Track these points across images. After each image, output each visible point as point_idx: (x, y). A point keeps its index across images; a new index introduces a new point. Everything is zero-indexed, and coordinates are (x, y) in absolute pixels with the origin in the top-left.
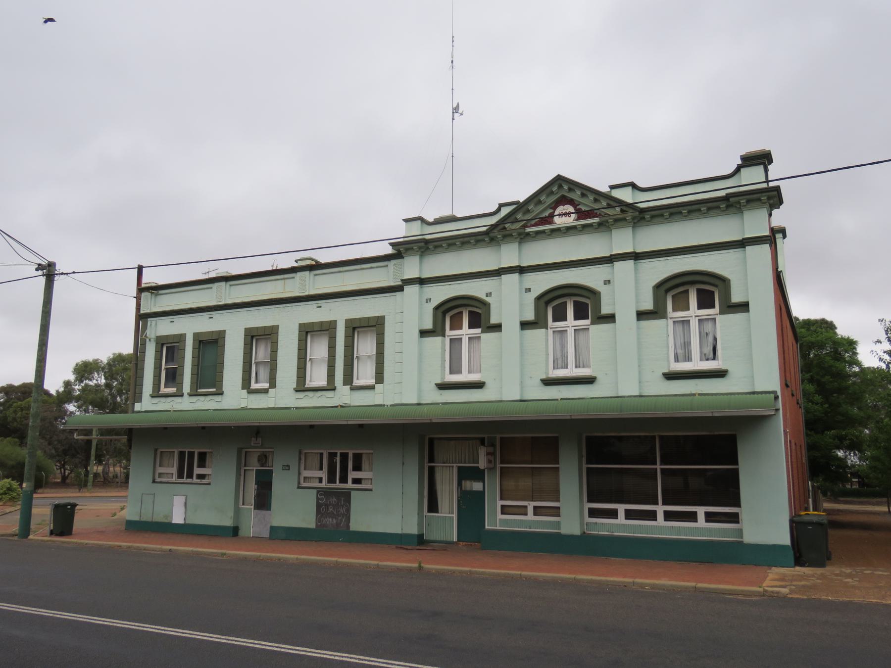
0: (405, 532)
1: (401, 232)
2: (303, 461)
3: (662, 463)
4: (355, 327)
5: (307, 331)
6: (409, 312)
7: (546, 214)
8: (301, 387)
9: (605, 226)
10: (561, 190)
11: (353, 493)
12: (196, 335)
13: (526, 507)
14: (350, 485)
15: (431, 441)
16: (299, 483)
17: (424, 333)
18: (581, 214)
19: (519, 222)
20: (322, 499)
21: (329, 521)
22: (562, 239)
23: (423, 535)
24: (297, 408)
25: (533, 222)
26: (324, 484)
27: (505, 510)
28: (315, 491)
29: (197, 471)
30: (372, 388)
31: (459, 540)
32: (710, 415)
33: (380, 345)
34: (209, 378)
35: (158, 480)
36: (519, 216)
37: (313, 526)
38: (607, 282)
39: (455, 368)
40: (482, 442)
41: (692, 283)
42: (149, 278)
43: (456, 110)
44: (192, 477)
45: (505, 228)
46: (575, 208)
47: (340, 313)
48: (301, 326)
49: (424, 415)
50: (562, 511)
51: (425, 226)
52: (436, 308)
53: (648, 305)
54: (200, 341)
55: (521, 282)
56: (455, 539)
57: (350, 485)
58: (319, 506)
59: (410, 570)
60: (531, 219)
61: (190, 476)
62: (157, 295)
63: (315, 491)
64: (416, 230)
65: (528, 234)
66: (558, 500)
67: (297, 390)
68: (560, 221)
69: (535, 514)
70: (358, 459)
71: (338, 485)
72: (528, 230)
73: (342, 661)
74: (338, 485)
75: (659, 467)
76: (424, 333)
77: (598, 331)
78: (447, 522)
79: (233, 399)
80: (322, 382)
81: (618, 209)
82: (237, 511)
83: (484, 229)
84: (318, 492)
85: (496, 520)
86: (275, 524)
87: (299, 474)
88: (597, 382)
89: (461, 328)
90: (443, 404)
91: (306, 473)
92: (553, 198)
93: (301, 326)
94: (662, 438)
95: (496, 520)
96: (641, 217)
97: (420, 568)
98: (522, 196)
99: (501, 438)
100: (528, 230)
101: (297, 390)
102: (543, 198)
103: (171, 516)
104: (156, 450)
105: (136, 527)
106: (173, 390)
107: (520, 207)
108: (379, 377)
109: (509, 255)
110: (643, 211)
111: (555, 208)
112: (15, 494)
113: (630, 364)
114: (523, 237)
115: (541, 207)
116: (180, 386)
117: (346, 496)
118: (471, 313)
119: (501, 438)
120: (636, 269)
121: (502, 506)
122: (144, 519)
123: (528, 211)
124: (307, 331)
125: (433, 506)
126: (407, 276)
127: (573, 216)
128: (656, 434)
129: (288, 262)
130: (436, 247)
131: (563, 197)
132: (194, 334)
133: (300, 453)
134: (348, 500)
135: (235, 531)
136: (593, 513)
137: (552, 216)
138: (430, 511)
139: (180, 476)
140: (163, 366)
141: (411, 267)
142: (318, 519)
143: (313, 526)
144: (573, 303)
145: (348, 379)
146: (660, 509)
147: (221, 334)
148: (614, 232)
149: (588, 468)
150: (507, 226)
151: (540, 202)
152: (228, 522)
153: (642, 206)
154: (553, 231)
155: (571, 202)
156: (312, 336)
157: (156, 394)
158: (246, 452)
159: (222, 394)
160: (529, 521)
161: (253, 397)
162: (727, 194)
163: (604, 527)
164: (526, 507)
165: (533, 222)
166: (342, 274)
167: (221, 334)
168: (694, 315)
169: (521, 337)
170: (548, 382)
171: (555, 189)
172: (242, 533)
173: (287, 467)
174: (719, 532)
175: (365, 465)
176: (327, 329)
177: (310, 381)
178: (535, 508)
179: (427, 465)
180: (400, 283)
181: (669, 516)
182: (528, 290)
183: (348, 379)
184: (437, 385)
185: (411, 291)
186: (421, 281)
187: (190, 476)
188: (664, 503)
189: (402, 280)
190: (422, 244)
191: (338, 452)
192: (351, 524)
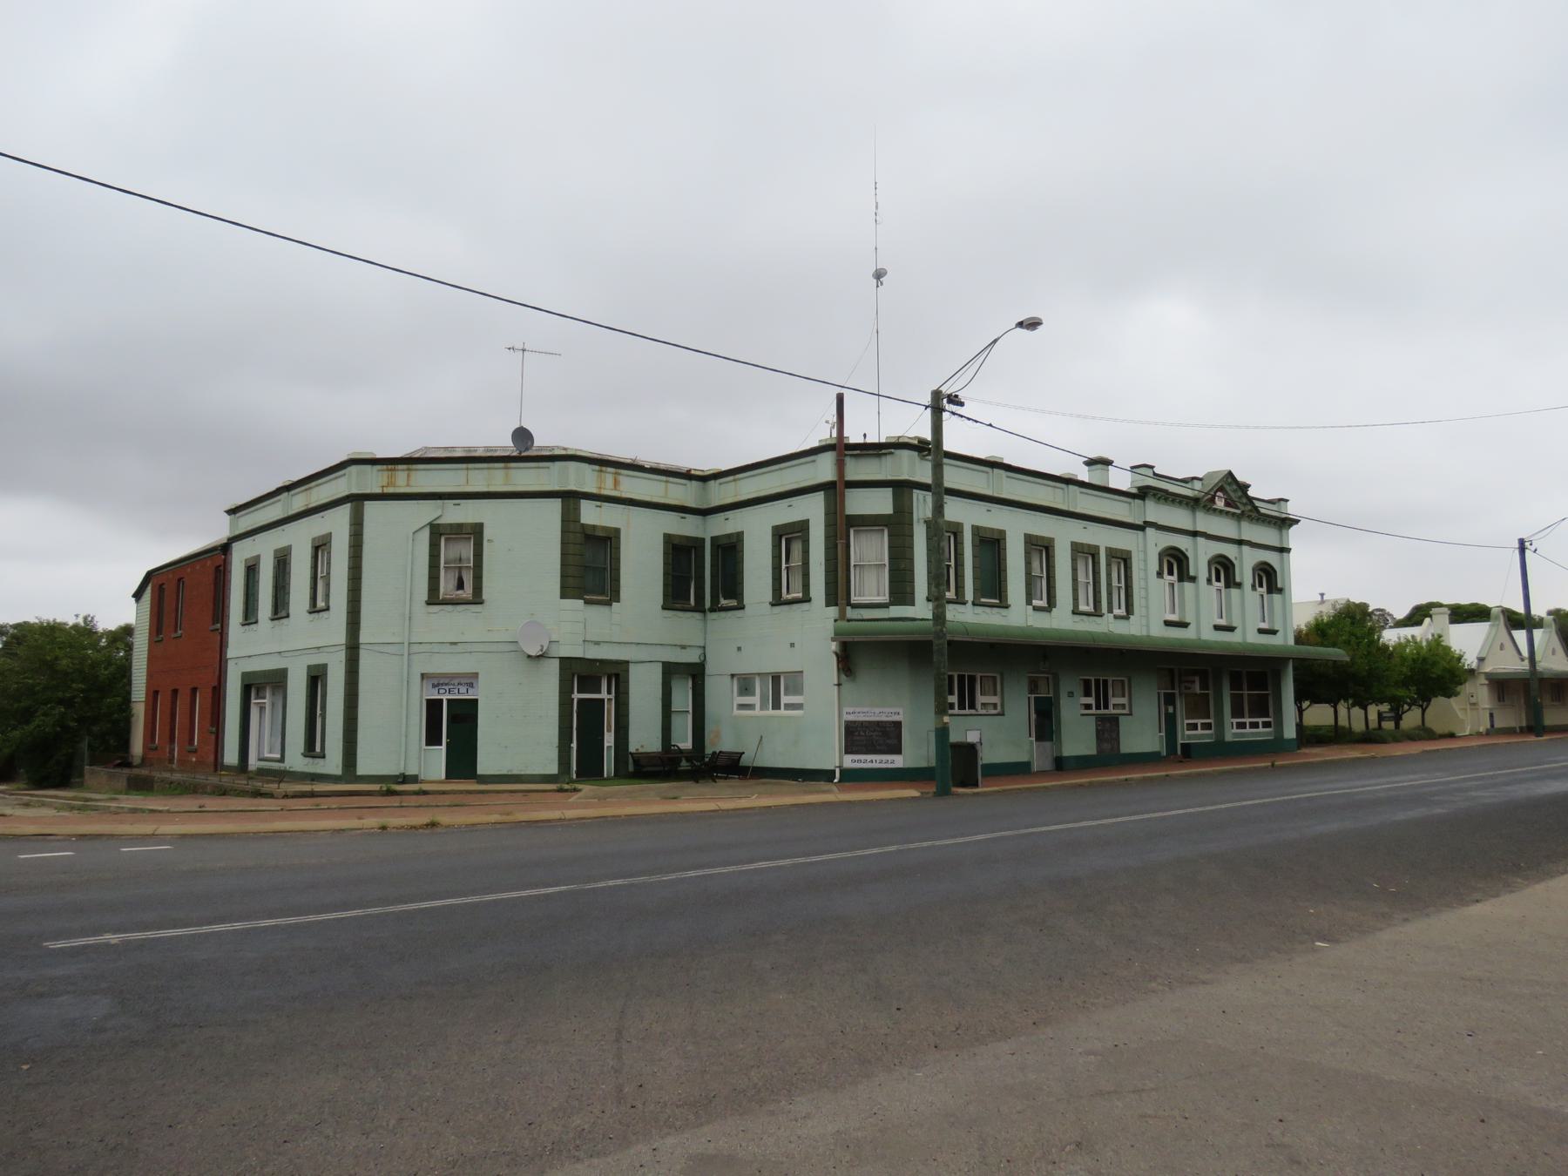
8: (1076, 612)
9: (1239, 518)
21: (1106, 746)
26: (1093, 711)
37: (1094, 752)
40: (1195, 673)
61: (972, 706)
67: (429, 603)
71: (1102, 711)
74: (771, 712)
79: (1018, 615)
80: (1090, 608)
117: (1115, 720)
126: (1150, 519)
139: (962, 707)
143: (1094, 752)
160: (1201, 735)
163: (1192, 732)
173: (1071, 694)
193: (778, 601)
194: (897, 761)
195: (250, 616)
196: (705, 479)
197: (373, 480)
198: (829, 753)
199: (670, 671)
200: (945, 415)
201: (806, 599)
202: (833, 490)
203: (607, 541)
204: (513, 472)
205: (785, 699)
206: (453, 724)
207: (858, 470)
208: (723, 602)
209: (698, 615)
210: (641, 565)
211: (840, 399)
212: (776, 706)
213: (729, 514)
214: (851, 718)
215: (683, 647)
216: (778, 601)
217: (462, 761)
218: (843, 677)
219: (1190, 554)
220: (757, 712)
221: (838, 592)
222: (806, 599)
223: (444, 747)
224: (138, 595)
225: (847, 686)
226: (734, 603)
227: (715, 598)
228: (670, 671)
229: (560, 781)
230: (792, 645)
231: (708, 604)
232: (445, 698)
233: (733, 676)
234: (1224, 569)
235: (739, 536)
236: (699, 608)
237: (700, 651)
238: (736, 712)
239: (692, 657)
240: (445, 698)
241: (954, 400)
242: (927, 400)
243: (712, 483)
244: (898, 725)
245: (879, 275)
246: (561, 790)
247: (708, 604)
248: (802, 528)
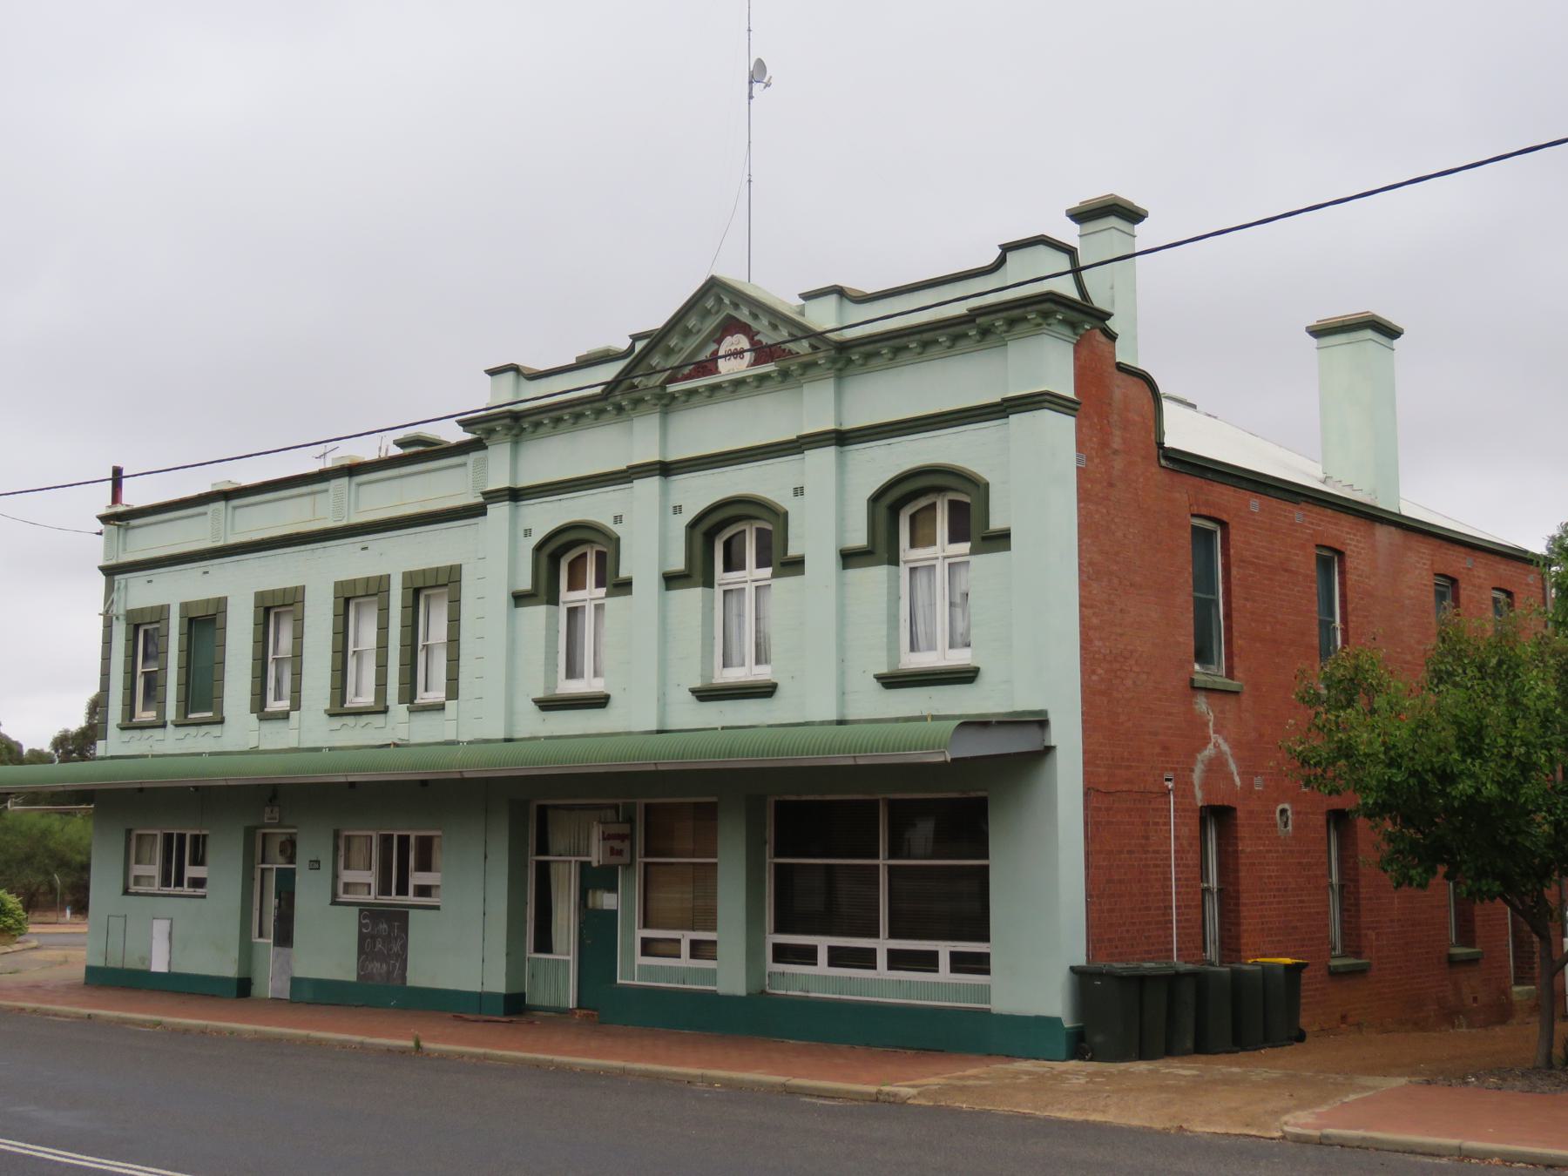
0: (486, 989)
1: (484, 396)
2: (342, 852)
3: (893, 854)
4: (419, 588)
5: (347, 598)
6: (494, 555)
7: (705, 354)
8: (339, 709)
10: (717, 308)
11: (412, 913)
12: (185, 607)
13: (678, 941)
14: (410, 898)
15: (543, 811)
16: (335, 894)
17: (519, 599)
18: (763, 353)
19: (652, 373)
20: (366, 926)
21: (377, 967)
22: (730, 404)
23: (523, 995)
24: (331, 749)
25: (686, 371)
26: (371, 898)
27: (648, 947)
28: (356, 910)
29: (191, 872)
30: (440, 707)
31: (579, 1007)
32: (851, 762)
33: (454, 621)
34: (201, 696)
35: (133, 889)
36: (655, 360)
37: (353, 977)
38: (799, 491)
39: (572, 672)
41: (940, 490)
42: (136, 495)
43: (758, 73)
44: (179, 883)
45: (634, 387)
46: (751, 339)
47: (396, 558)
48: (339, 586)
49: (664, 755)
50: (720, 950)
51: (523, 381)
52: (692, 526)
53: (858, 537)
54: (191, 620)
55: (664, 493)
56: (572, 1003)
57: (410, 898)
59: (403, 1052)
60: (680, 367)
62: (127, 529)
63: (356, 910)
64: (502, 394)
65: (673, 397)
66: (714, 929)
68: (730, 368)
69: (693, 956)
70: (426, 845)
71: (394, 899)
72: (672, 388)
73: (57, 1163)
75: (883, 862)
76: (519, 599)
77: (784, 586)
78: (559, 976)
80: (368, 699)
81: (805, 343)
82: (247, 951)
83: (598, 390)
84: (361, 911)
85: (635, 969)
86: (299, 973)
87: (336, 877)
88: (779, 693)
89: (584, 587)
90: (546, 738)
91: (347, 876)
92: (711, 323)
93: (339, 586)
94: (893, 805)
95: (635, 969)
96: (847, 357)
98: (657, 321)
99: (647, 806)
100: (672, 388)
101: (123, 729)
102: (692, 322)
103: (147, 958)
104: (129, 832)
105: (103, 979)
106: (150, 716)
107: (656, 340)
108: (453, 692)
109: (639, 440)
110: (843, 347)
111: (719, 342)
112: (11, 921)
113: (825, 662)
114: (667, 404)
115: (693, 342)
116: (162, 712)
117: (400, 918)
118: (952, 504)
119: (647, 806)
120: (841, 466)
121: (776, 947)
122: (111, 965)
123: (669, 352)
124: (347, 598)
125: (544, 943)
127: (748, 356)
128: (880, 797)
129: (307, 463)
130: (868, 357)
131: (730, 318)
132: (257, 594)
133: (337, 835)
134: (404, 929)
135: (243, 987)
136: (783, 954)
137: (715, 357)
138: (537, 950)
139: (166, 882)
140: (140, 669)
141: (499, 466)
142: (361, 966)
143: (353, 977)
144: (737, 536)
145: (409, 693)
146: (882, 945)
147: (221, 604)
148: (805, 386)
149: (777, 866)
150: (636, 381)
151: (687, 333)
152: (230, 970)
154: (714, 389)
155: (745, 329)
156: (358, 606)
157: (129, 724)
158: (264, 835)
159: (222, 722)
160: (678, 971)
161: (269, 727)
162: (971, 310)
163: (820, 979)
164: (678, 941)
165: (686, 371)
166: (395, 483)
167: (221, 604)
168: (940, 554)
169: (841, 585)
170: (893, 681)
171: (710, 303)
172: (256, 991)
173: (315, 865)
174: (940, 986)
175: (438, 858)
176: (376, 589)
177: (357, 695)
178: (831, 949)
179: (533, 859)
180: (481, 499)
181: (898, 960)
182: (678, 510)
183: (409, 693)
184: (536, 701)
185: (499, 512)
186: (515, 495)
188: (893, 935)
189: (484, 494)
190: (507, 421)
192: (408, 974)
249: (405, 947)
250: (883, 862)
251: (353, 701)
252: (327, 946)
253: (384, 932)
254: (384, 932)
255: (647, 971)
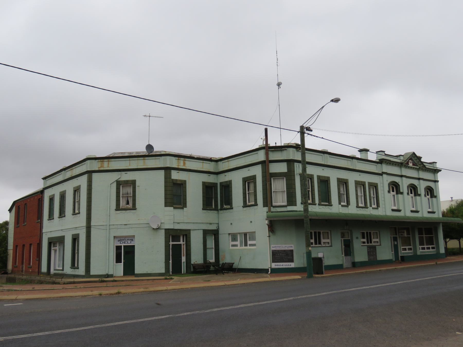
6: (383, 183)
8: (358, 207)
26: (366, 244)
34: (326, 198)
37: (367, 260)
40: (404, 229)
47: (367, 179)
58: (368, 252)
61: (320, 243)
74: (244, 247)
79: (336, 209)
80: (363, 205)
97: (436, 264)
139: (316, 244)
143: (367, 260)
153: (427, 167)
159: (232, 209)
163: (404, 252)
173: (357, 238)
187: (320, 243)
188: (181, 244)
191: (322, 232)
193: (245, 206)
194: (292, 265)
195: (51, 217)
196: (217, 161)
197: (95, 166)
198: (266, 262)
199: (206, 233)
200: (305, 135)
201: (256, 205)
202: (265, 164)
203: (182, 185)
204: (146, 161)
205: (249, 242)
206: (126, 255)
207: (274, 156)
208: (225, 206)
209: (216, 212)
210: (194, 194)
211: (266, 130)
212: (246, 245)
213: (226, 174)
214: (274, 249)
215: (211, 224)
216: (245, 206)
217: (129, 269)
218: (271, 233)
219: (400, 184)
220: (239, 247)
221: (268, 202)
222: (256, 205)
223: (122, 264)
224: (10, 210)
225: (272, 237)
226: (229, 207)
227: (222, 206)
228: (206, 233)
229: (166, 275)
230: (251, 222)
231: (219, 207)
232: (122, 245)
233: (229, 234)
234: (413, 189)
235: (230, 182)
236: (216, 209)
237: (217, 225)
238: (231, 248)
239: (214, 227)
240: (122, 245)
241: (309, 129)
242: (298, 129)
243: (220, 162)
244: (292, 251)
245: (279, 84)
246: (166, 279)
247: (219, 207)
248: (253, 178)
249: (376, 253)
250: (424, 236)
251: (360, 205)
252: (361, 254)
253: (372, 251)
254: (372, 251)
255: (421, 252)
